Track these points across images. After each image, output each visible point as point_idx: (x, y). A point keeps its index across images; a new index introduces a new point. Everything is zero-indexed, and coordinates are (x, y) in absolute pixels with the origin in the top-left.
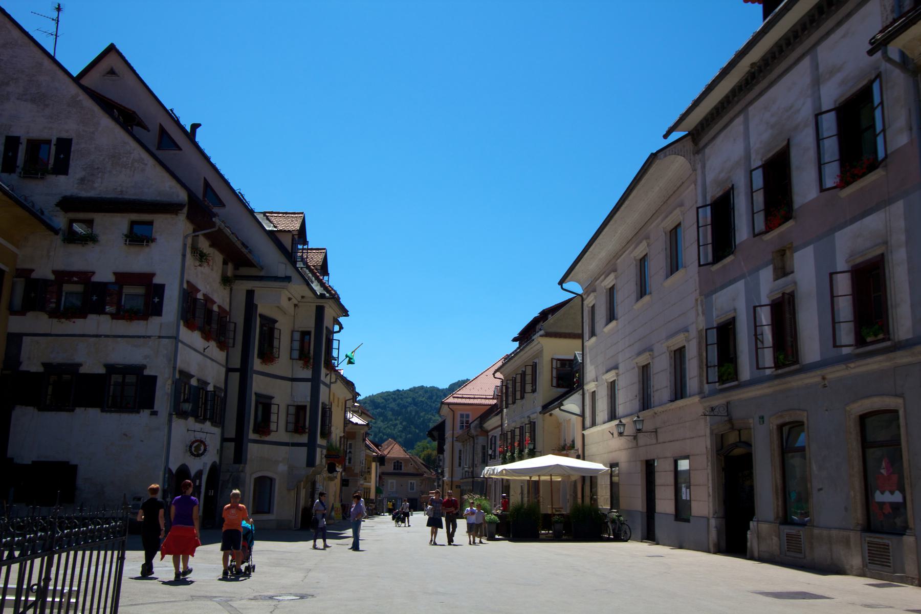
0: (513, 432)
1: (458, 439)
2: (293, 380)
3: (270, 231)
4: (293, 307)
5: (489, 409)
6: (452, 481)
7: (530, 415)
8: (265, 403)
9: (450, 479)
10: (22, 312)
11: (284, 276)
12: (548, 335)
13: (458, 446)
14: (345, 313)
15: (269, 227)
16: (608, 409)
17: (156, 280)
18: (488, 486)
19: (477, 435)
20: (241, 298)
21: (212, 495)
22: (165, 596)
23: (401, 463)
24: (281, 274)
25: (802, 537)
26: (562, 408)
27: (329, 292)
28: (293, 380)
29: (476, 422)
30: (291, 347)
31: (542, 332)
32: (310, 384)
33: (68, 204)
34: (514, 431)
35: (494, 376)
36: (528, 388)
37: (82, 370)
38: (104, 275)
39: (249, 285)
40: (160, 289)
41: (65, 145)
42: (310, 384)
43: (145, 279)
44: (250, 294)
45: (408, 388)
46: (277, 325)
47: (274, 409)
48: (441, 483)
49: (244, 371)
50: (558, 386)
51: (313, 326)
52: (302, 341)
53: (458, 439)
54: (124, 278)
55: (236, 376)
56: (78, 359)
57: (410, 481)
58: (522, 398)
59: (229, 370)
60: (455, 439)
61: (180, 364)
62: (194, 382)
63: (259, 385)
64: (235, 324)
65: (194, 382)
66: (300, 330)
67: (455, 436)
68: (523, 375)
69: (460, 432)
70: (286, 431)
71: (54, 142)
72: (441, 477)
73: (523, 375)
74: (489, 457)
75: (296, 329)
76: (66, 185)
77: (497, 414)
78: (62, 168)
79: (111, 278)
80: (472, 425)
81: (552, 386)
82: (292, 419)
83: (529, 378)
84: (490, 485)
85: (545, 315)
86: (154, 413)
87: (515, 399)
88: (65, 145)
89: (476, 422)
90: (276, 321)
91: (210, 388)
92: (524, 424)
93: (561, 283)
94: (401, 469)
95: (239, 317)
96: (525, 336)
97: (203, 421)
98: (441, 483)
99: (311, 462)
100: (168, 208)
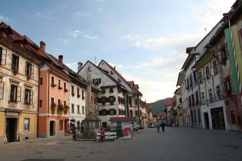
2: (135, 107)
4: (139, 135)
7: (188, 95)
8: (131, 111)
17: (114, 97)
20: (126, 96)
22: (80, 139)
24: (131, 91)
28: (135, 107)
33: (102, 88)
37: (107, 110)
38: (107, 97)
40: (115, 98)
41: (100, 79)
43: (113, 97)
45: (154, 102)
47: (133, 112)
49: (128, 107)
52: (136, 112)
54: (110, 97)
55: (127, 107)
56: (106, 109)
59: (125, 107)
61: (119, 108)
62: (121, 110)
63: (130, 108)
65: (121, 110)
68: (191, 77)
76: (101, 85)
78: (100, 82)
79: (108, 97)
82: (136, 113)
83: (193, 77)
86: (116, 115)
88: (100, 79)
91: (123, 110)
95: (126, 99)
97: (123, 115)
100: (114, 87)
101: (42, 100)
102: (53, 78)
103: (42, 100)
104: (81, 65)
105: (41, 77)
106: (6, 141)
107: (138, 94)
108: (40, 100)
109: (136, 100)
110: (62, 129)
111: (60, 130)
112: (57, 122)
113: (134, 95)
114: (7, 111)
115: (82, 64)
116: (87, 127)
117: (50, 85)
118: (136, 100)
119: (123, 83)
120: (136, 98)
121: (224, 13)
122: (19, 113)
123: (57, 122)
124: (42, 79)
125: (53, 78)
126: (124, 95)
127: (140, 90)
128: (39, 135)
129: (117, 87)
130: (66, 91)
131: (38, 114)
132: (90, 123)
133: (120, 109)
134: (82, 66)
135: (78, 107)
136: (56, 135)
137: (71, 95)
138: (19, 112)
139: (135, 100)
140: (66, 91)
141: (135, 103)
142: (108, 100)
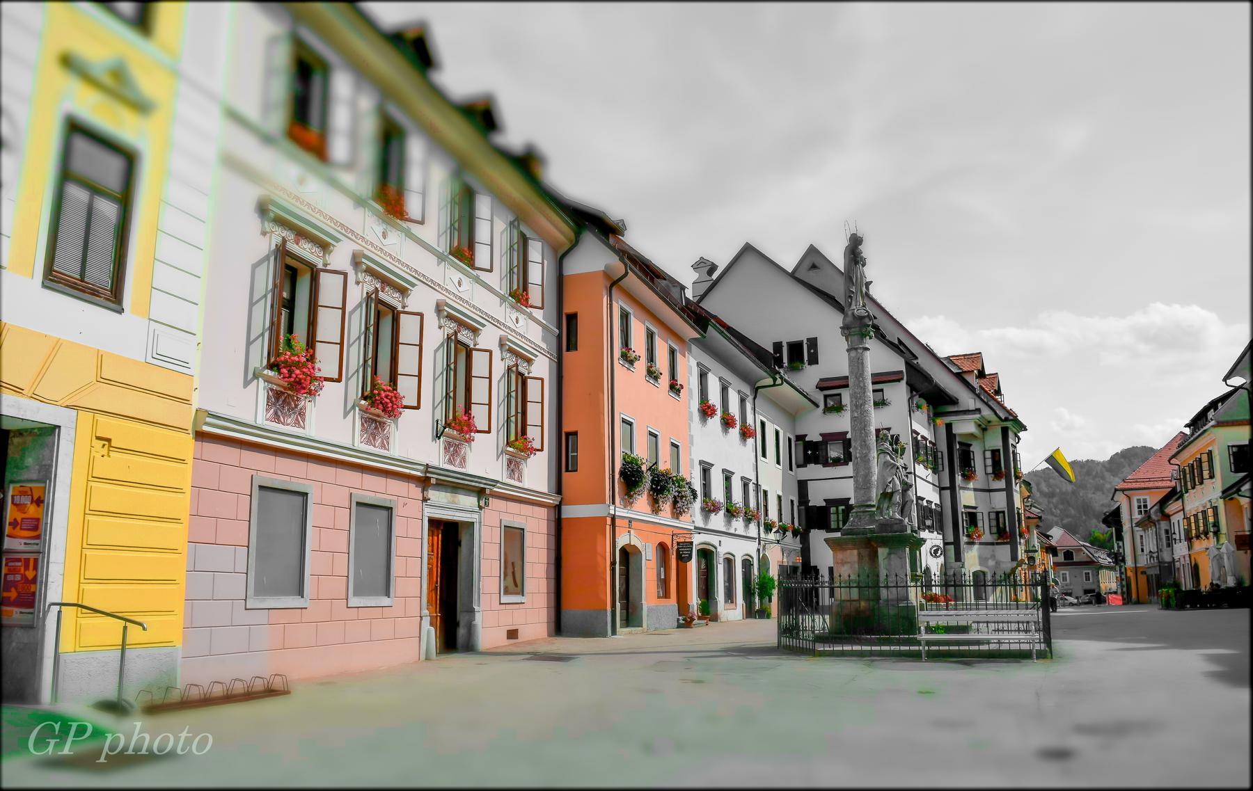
0: (1196, 516)
1: (1138, 525)
3: (957, 373)
5: (1170, 492)
6: (1136, 567)
9: (1134, 566)
10: (804, 465)
11: (974, 409)
12: (1220, 424)
13: (1139, 531)
14: (1023, 428)
15: (955, 370)
16: (910, 661)
18: (1176, 569)
19: (1158, 521)
20: (943, 431)
21: (800, 616)
23: (1072, 553)
24: (972, 407)
25: (195, 370)
26: (1240, 493)
27: (1011, 414)
28: (990, 491)
29: (1156, 508)
30: (985, 464)
31: (1212, 423)
32: (1005, 492)
34: (1197, 514)
35: (1169, 462)
36: (1206, 474)
39: (948, 419)
41: (813, 343)
42: (1005, 492)
44: (949, 427)
46: (971, 449)
48: (1123, 570)
50: (1237, 471)
51: (1001, 444)
52: (997, 519)
53: (1138, 525)
54: (828, 438)
55: (948, 493)
57: (1085, 571)
58: (1201, 483)
59: (942, 489)
60: (1134, 525)
62: (925, 503)
63: (967, 498)
64: (942, 452)
66: (991, 449)
67: (1134, 522)
69: (1140, 517)
70: (991, 533)
71: (805, 342)
72: (1122, 564)
73: (1200, 461)
74: (1174, 541)
75: (987, 449)
77: (1177, 500)
80: (1152, 511)
81: (1231, 471)
84: (1178, 569)
85: (1213, 405)
87: (1195, 484)
89: (1156, 508)
90: (970, 445)
92: (1206, 509)
93: (1225, 380)
94: (1073, 559)
95: (943, 447)
96: (1198, 421)
98: (1123, 570)
99: (1014, 557)
100: (893, 378)
101: (575, 434)
102: (625, 317)
103: (575, 434)
104: (711, 272)
105: (568, 309)
106: (1213, 574)
107: (1006, 419)
108: (568, 434)
109: (995, 453)
110: (666, 595)
111: (659, 597)
112: (649, 556)
113: (984, 430)
114: (433, 481)
115: (713, 268)
116: (853, 577)
117: (617, 354)
118: (995, 453)
119: (924, 362)
120: (998, 444)
121: (242, 386)
122: (480, 493)
123: (649, 556)
124: (572, 318)
125: (625, 317)
126: (932, 420)
127: (1011, 400)
128: (569, 613)
129: (904, 382)
130: (675, 388)
131: (558, 508)
132: (882, 552)
133: (923, 499)
134: (715, 276)
135: (728, 477)
136: (645, 625)
137: (696, 416)
138: (481, 491)
139: (988, 454)
140: (675, 388)
141: (990, 470)
142: (814, 453)
